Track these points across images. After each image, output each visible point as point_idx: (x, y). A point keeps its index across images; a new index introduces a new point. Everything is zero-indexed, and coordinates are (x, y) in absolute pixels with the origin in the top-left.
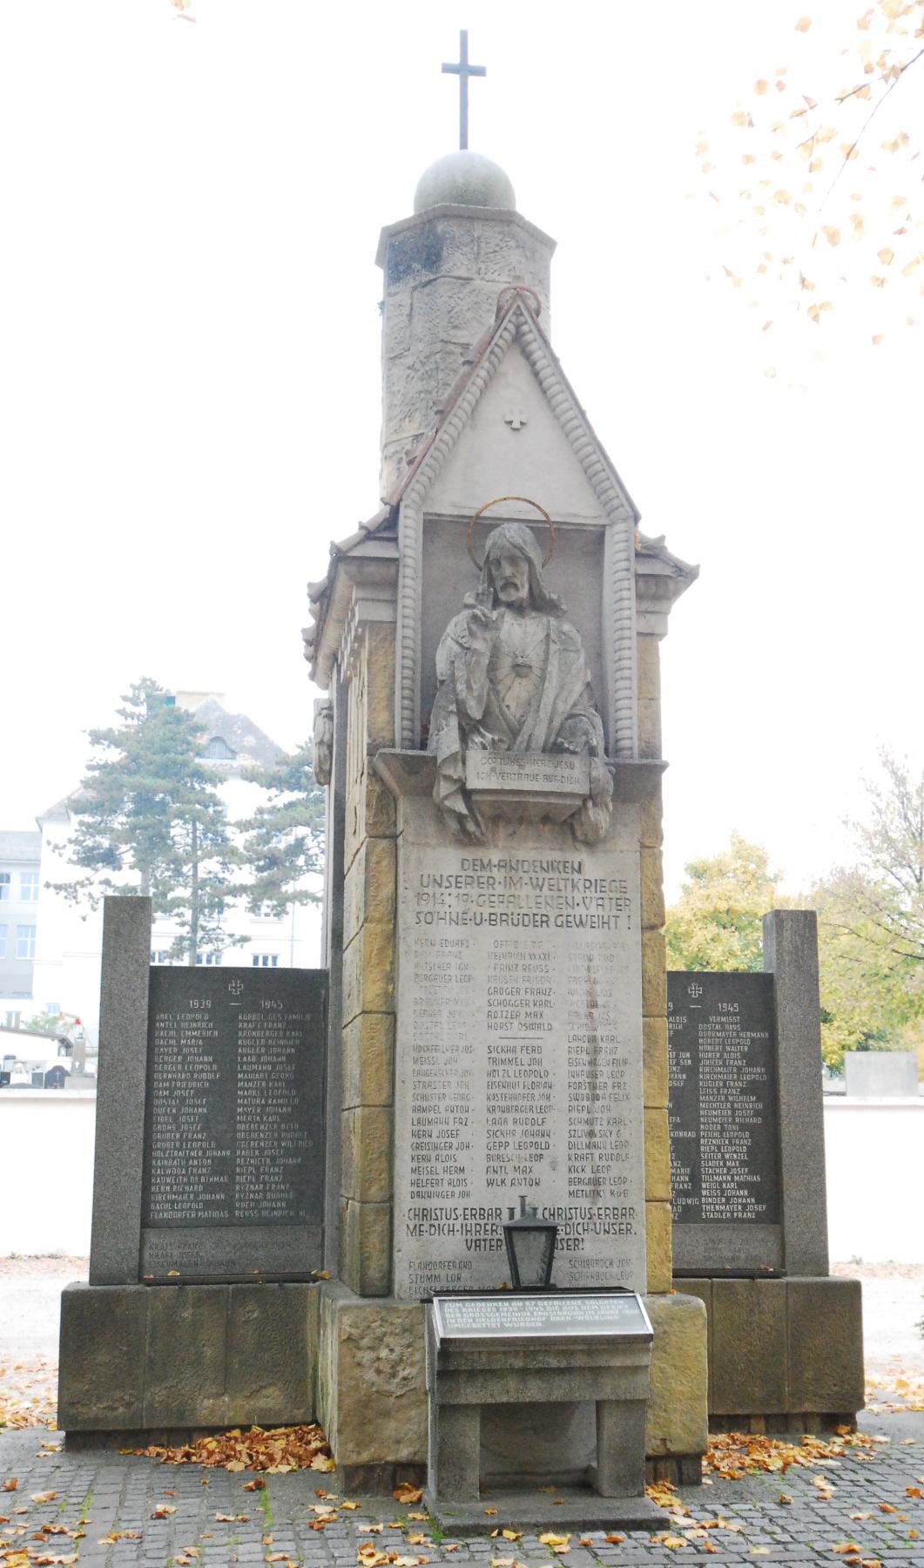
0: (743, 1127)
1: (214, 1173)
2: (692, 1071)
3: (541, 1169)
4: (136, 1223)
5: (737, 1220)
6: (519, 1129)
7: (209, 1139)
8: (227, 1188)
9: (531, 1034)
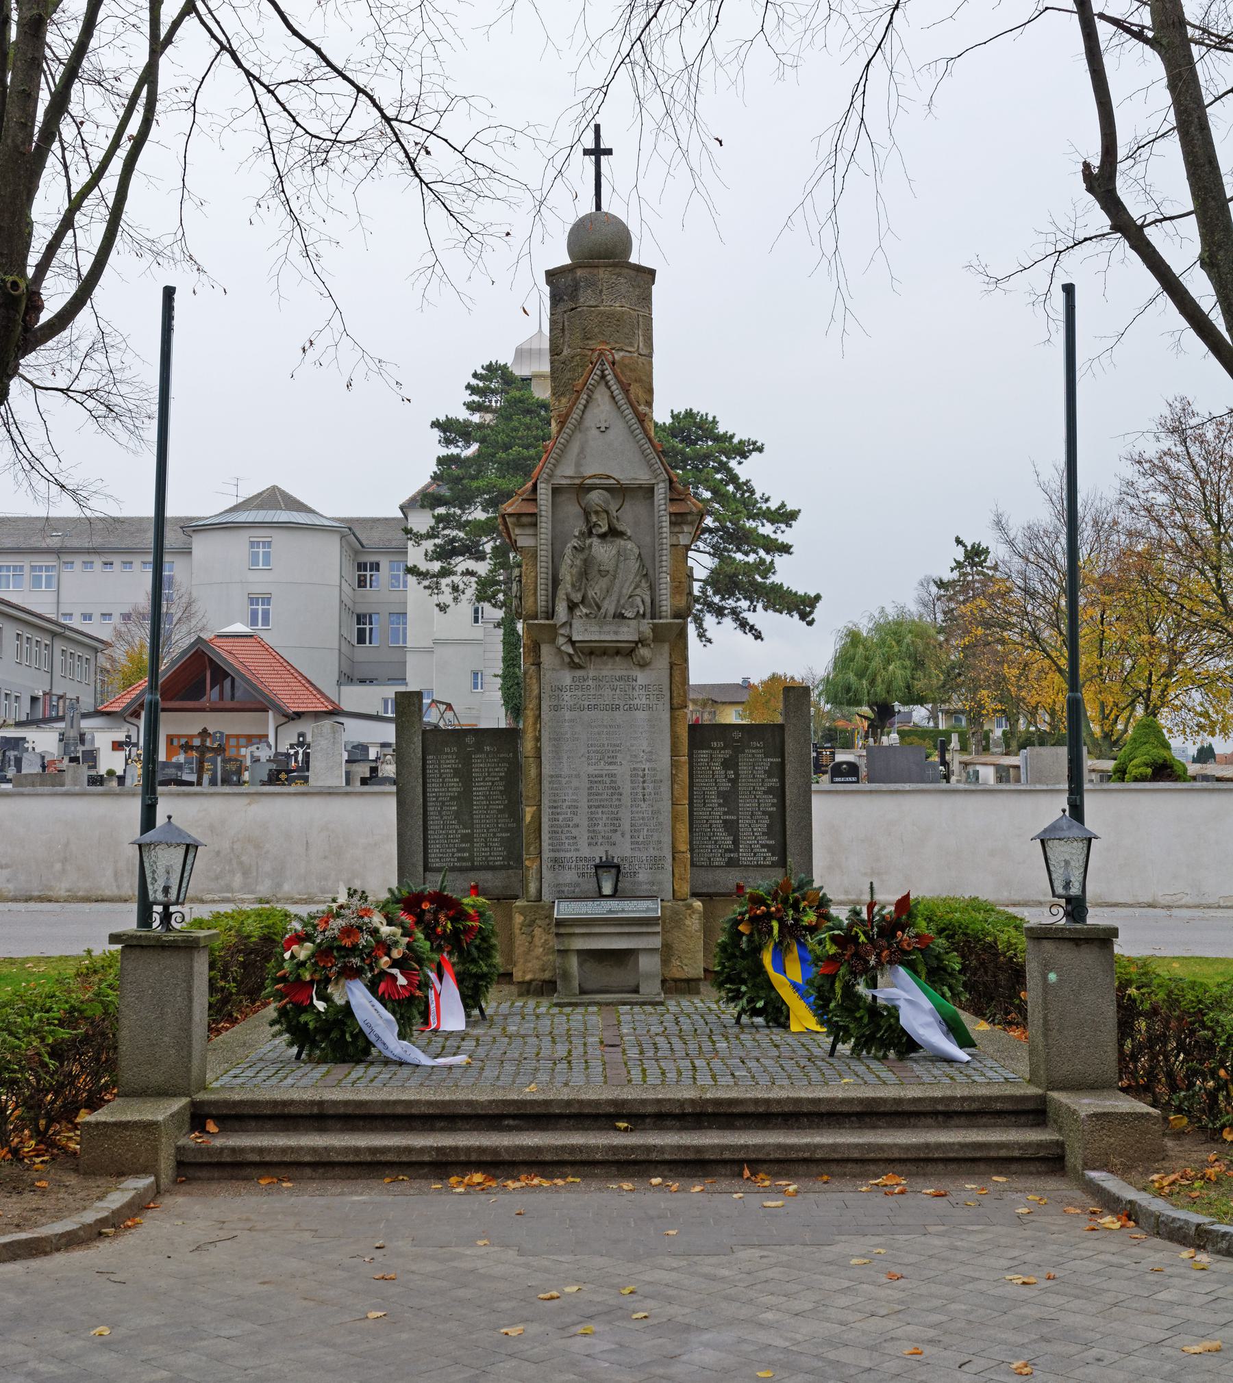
0: (764, 813)
1: (462, 842)
2: (734, 782)
3: (616, 837)
4: (421, 869)
5: (761, 866)
6: (604, 816)
7: (459, 823)
8: (470, 850)
9: (611, 767)
